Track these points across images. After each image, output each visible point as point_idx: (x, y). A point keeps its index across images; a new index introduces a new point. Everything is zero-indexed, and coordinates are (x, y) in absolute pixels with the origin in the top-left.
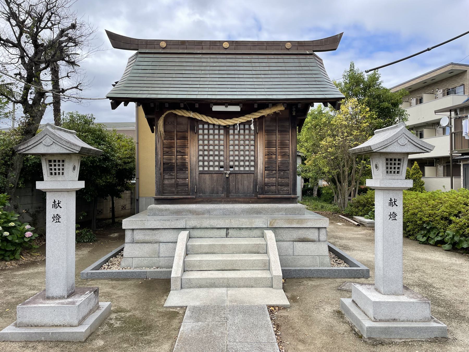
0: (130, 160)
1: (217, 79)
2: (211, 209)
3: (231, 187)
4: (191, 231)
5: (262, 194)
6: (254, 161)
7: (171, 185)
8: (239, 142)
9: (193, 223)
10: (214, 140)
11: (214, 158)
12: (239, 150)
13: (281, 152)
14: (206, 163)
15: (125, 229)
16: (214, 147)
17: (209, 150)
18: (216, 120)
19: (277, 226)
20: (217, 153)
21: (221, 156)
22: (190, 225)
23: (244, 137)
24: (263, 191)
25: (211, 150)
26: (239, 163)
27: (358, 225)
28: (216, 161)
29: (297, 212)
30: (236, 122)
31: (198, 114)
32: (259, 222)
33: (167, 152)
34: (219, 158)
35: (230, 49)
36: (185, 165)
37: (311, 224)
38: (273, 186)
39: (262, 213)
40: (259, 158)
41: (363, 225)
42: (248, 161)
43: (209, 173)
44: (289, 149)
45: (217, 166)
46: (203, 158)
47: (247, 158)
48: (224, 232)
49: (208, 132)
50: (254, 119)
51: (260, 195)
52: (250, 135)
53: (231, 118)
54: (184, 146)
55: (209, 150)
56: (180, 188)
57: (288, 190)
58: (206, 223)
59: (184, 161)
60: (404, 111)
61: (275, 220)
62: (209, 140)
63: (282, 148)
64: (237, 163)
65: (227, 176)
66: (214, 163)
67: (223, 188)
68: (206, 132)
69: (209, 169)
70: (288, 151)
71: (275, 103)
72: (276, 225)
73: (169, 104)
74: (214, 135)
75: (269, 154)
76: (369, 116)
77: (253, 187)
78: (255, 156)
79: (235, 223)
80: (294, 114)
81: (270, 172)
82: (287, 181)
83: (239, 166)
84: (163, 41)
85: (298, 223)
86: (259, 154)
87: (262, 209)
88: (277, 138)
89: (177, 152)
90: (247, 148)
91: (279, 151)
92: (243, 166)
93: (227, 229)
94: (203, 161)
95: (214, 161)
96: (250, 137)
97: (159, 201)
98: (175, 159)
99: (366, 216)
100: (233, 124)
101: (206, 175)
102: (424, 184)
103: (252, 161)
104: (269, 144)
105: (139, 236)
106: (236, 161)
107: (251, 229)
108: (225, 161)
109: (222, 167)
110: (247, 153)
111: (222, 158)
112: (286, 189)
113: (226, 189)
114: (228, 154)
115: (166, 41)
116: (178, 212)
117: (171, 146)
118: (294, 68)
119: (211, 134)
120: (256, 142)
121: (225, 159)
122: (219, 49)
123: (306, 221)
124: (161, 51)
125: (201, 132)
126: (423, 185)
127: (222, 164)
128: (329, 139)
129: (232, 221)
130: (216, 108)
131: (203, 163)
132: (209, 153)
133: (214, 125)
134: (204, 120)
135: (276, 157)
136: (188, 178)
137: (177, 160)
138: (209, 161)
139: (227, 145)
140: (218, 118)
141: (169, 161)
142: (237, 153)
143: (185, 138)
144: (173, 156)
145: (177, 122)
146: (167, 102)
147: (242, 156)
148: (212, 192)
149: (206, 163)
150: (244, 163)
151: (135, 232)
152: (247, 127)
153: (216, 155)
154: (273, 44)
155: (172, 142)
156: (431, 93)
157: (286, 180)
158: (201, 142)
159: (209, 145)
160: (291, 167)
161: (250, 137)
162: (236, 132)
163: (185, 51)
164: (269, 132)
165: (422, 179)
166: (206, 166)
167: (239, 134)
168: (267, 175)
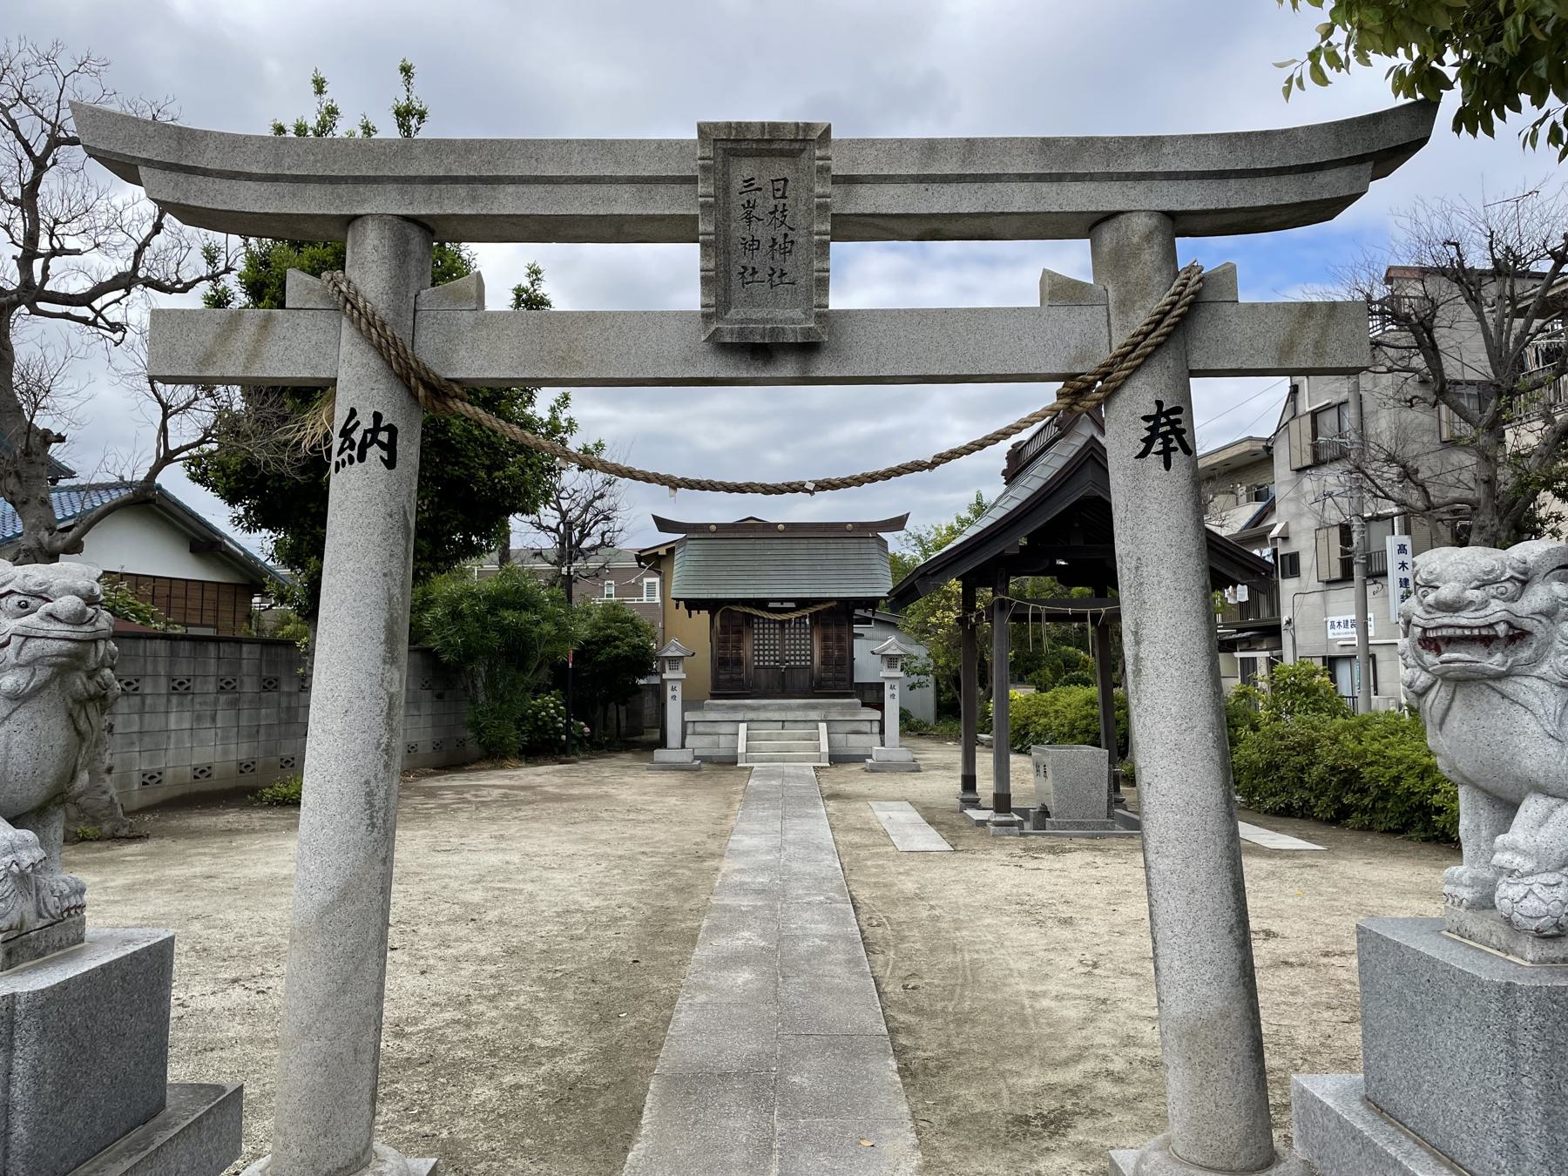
9: (751, 715)
24: (819, 686)
32: (813, 715)
43: (764, 667)
54: (740, 641)
75: (825, 649)
78: (812, 650)
79: (790, 716)
88: (833, 631)
97: (714, 696)
98: (730, 654)
104: (825, 638)
105: (700, 728)
117: (725, 641)
139: (782, 640)
143: (739, 632)
164: (825, 625)
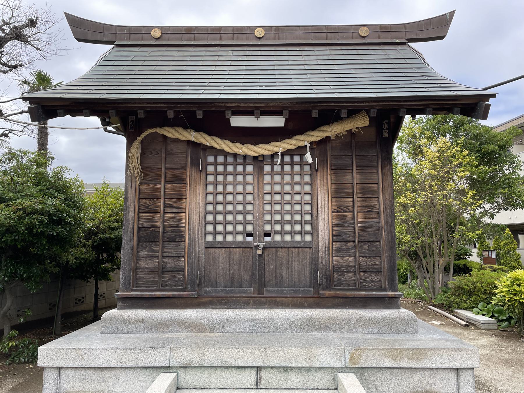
0: (116, 225)
1: (243, 76)
2: (228, 320)
3: (267, 273)
4: (182, 372)
5: (329, 287)
6: (311, 223)
7: (152, 271)
8: (282, 188)
9: (183, 356)
10: (235, 184)
11: (235, 218)
12: (281, 203)
13: (363, 207)
14: (220, 228)
15: (42, 368)
16: (235, 198)
17: (226, 203)
18: (239, 145)
19: (366, 365)
20: (240, 208)
21: (249, 213)
22: (179, 359)
23: (292, 179)
24: (330, 284)
25: (230, 203)
26: (282, 228)
27: (466, 325)
28: (240, 223)
29: (402, 328)
30: (276, 150)
31: (205, 135)
32: (327, 356)
33: (147, 207)
34: (245, 218)
35: (267, 39)
36: (181, 231)
37: (442, 360)
38: (350, 272)
39: (330, 329)
40: (320, 218)
41: (474, 325)
42: (300, 223)
43: (225, 246)
44: (378, 201)
45: (239, 233)
46: (215, 218)
47: (298, 218)
48: (250, 377)
49: (225, 168)
50: (312, 143)
51: (324, 289)
52: (302, 174)
53: (267, 143)
54: (180, 196)
55: (226, 203)
56: (168, 277)
57: (380, 281)
58: (213, 356)
59: (177, 224)
60: (515, 157)
61: (363, 350)
62: (225, 184)
63: (363, 199)
64: (278, 228)
65: (260, 252)
66: (234, 228)
67: (252, 276)
68: (220, 168)
69: (224, 238)
70: (376, 203)
71: (354, 107)
72: (363, 363)
73: (147, 112)
74: (235, 174)
75: (338, 211)
76: (468, 163)
77: (311, 273)
79: (274, 356)
80: (386, 135)
81: (343, 244)
82: (377, 263)
83: (283, 233)
84: (156, 27)
85: (411, 357)
86: (320, 210)
87: (329, 319)
89: (165, 206)
90: (297, 198)
91: (358, 204)
92: (290, 233)
93: (259, 369)
94: (215, 223)
95: (235, 223)
96: (302, 178)
98: (161, 219)
99: (474, 309)
100: (271, 153)
101: (220, 250)
102: (520, 258)
103: (306, 223)
104: (339, 192)
106: (277, 222)
107: (309, 369)
108: (256, 224)
109: (249, 235)
110: (298, 208)
111: (249, 218)
112: (375, 278)
113: (258, 278)
114: (261, 210)
115: (161, 28)
116: (161, 326)
118: (379, 61)
119: (230, 174)
120: (314, 186)
121: (256, 220)
122: (248, 39)
123: (430, 353)
124: (152, 42)
125: (211, 169)
126: (518, 259)
127: (249, 228)
128: (409, 195)
129: (269, 351)
130: (238, 122)
131: (215, 228)
132: (225, 207)
133: (235, 155)
134: (216, 146)
135: (354, 215)
136: (184, 257)
137: (164, 221)
138: (225, 223)
139: (259, 194)
140: (243, 143)
141: (149, 224)
142: (278, 208)
144: (158, 215)
145: (167, 150)
146: (141, 108)
147: (288, 213)
148: (231, 284)
149: (220, 228)
150: (293, 227)
151: (64, 374)
152: (297, 159)
153: (239, 212)
154: (338, 29)
155: (157, 189)
156: (519, 144)
157: (372, 262)
158: (210, 188)
159: (225, 194)
160: (384, 235)
161: (302, 178)
162: (277, 168)
163: (193, 43)
164: (338, 169)
165: (518, 251)
166: (219, 233)
167: (282, 173)
168: (337, 251)
